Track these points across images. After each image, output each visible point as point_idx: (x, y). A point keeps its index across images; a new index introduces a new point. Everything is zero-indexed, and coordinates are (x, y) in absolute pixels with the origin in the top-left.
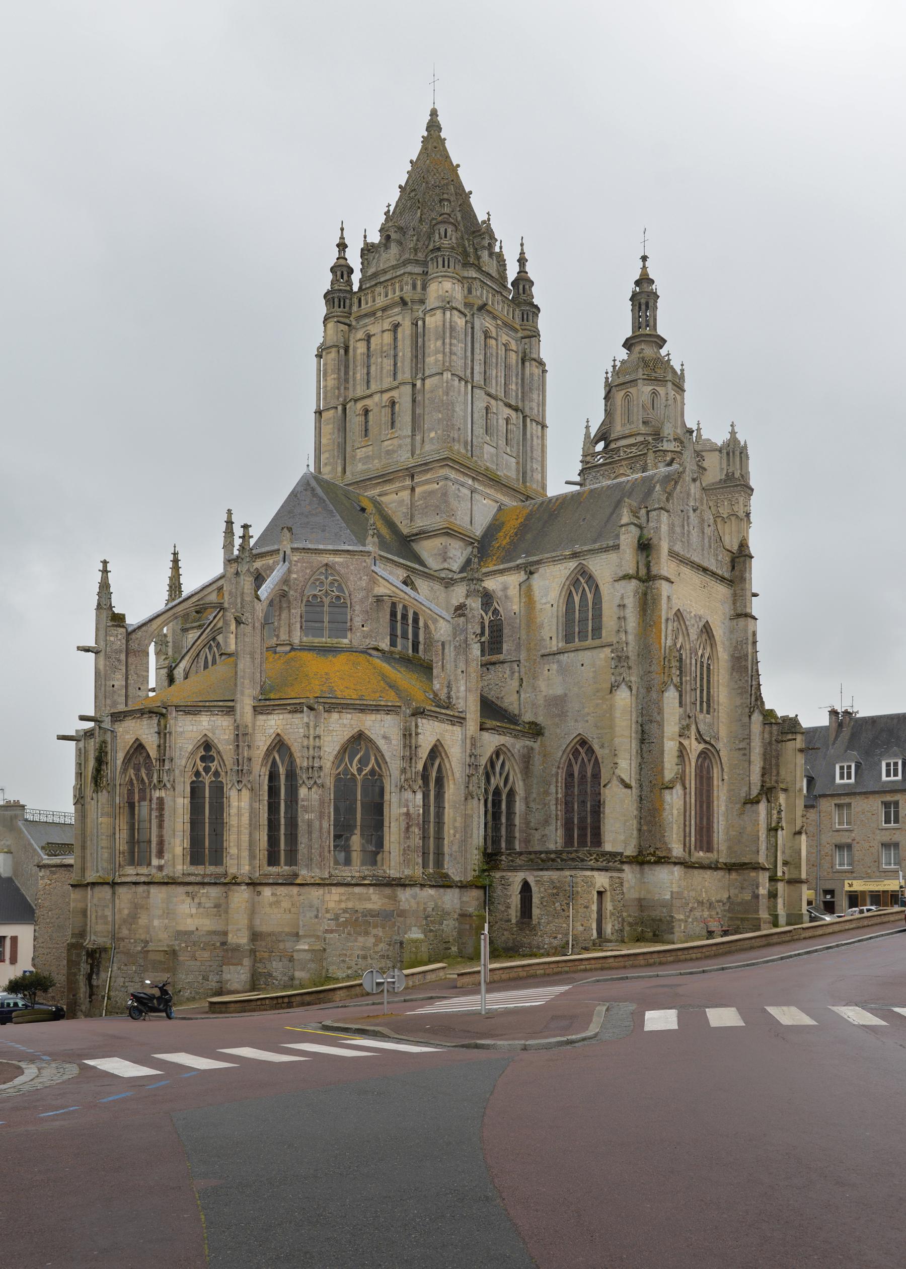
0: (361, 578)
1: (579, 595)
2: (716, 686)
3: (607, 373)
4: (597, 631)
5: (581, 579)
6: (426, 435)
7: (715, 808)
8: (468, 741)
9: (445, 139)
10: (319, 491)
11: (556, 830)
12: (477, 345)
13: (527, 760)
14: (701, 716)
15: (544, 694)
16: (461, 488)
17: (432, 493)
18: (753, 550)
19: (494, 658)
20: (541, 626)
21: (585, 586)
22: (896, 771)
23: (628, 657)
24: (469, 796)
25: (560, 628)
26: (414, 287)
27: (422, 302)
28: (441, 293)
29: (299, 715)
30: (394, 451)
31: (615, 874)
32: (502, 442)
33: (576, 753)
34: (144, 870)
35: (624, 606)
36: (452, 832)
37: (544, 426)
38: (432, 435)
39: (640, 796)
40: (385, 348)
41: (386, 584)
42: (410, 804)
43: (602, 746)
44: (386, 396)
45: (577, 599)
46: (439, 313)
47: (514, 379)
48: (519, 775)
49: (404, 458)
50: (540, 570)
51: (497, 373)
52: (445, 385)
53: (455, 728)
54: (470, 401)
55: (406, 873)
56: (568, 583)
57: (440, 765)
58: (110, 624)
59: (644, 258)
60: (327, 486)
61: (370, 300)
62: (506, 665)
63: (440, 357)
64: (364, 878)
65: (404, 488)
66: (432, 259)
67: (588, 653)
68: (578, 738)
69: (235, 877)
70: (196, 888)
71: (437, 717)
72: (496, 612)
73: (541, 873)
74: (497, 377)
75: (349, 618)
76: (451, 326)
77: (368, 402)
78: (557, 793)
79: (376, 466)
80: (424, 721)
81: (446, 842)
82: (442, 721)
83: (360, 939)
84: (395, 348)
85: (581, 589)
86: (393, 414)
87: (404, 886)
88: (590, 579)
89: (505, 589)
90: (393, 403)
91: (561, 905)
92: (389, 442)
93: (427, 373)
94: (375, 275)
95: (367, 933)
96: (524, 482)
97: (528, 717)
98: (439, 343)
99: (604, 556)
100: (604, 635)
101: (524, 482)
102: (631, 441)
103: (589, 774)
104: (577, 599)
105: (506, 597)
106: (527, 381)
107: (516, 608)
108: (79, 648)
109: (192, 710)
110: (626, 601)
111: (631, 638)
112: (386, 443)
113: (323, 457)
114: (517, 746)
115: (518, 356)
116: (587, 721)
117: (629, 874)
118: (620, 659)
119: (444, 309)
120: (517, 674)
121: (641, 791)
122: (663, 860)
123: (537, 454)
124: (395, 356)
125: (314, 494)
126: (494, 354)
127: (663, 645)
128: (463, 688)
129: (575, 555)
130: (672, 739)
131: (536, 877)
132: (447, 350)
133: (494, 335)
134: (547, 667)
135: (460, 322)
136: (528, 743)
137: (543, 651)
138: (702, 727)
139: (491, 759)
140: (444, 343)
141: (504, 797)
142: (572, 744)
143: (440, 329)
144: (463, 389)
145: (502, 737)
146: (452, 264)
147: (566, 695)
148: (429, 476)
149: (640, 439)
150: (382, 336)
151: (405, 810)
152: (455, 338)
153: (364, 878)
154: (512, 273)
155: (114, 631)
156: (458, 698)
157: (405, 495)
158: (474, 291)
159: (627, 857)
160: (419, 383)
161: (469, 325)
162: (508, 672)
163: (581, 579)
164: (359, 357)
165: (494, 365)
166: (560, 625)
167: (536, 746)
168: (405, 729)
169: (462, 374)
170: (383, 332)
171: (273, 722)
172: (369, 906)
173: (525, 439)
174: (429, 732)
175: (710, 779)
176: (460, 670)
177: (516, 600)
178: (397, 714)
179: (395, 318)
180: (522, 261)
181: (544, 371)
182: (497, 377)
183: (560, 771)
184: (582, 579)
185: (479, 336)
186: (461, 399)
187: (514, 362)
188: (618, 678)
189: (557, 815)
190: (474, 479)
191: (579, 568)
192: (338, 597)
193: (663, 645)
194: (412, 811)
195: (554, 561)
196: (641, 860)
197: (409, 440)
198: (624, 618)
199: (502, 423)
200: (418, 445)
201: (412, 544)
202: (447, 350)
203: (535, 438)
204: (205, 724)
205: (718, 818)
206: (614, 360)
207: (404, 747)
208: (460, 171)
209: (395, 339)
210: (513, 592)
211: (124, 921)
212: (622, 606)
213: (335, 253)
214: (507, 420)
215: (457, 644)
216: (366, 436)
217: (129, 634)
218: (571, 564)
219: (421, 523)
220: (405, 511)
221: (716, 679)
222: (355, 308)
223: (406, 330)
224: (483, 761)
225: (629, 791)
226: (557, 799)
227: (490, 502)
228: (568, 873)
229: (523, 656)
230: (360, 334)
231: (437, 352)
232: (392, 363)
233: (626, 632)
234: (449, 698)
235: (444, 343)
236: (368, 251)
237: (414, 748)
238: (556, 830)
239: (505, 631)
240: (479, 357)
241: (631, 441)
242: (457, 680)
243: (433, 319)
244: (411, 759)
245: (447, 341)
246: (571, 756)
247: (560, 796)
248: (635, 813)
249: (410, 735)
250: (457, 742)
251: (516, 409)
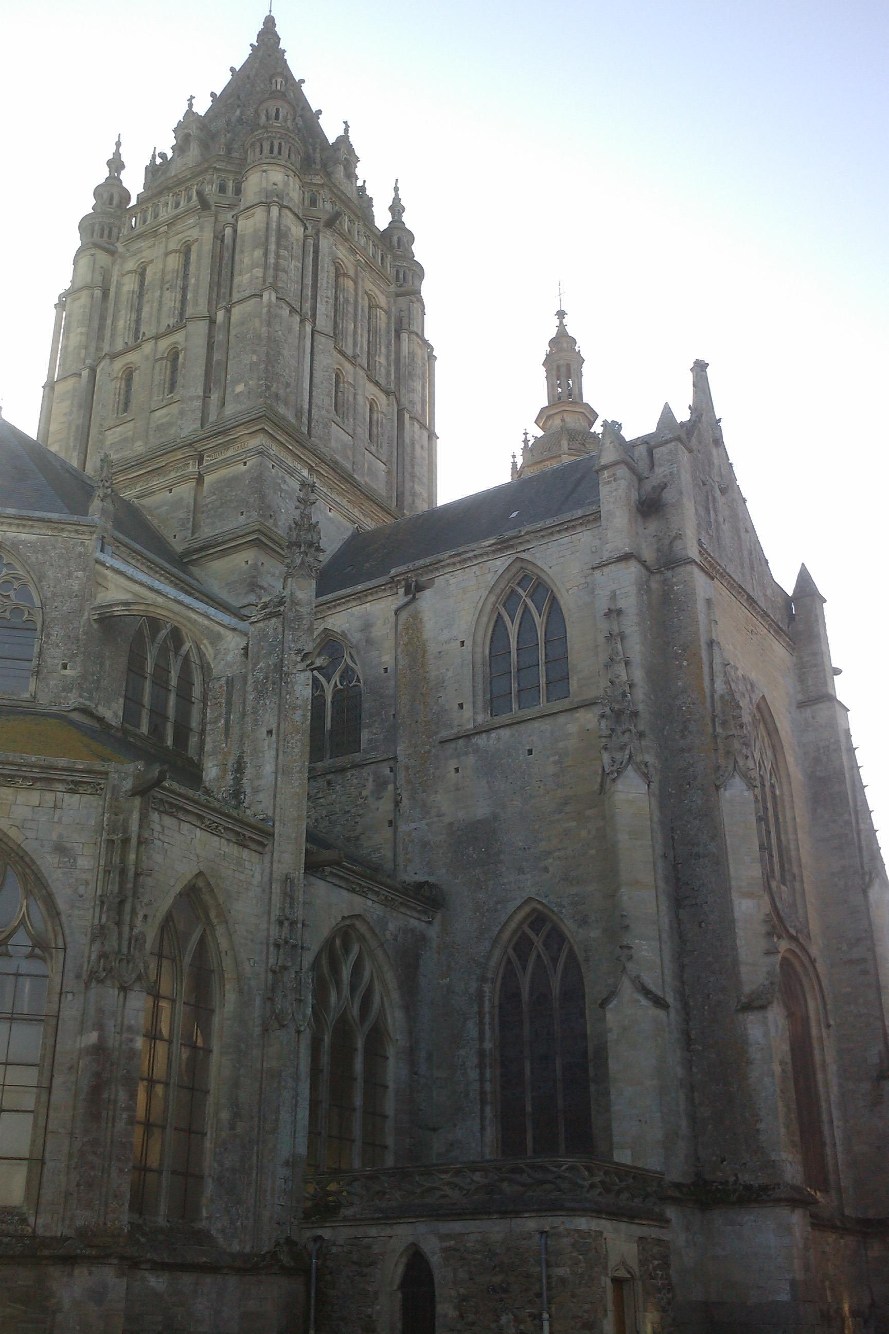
0: (70, 575)
1: (517, 620)
2: (790, 829)
3: (514, 457)
4: (559, 679)
5: (520, 590)
6: (228, 391)
7: (821, 1089)
8: (276, 888)
9: (284, 51)
11: (483, 1129)
13: (409, 960)
15: (447, 820)
16: (287, 477)
17: (233, 481)
18: (822, 590)
21: (529, 601)
23: (635, 714)
24: (274, 1021)
25: (480, 686)
26: (222, 189)
28: (264, 185)
31: (654, 1233)
33: (522, 946)
35: (619, 612)
36: (225, 1115)
38: (240, 388)
39: (686, 1034)
40: (167, 278)
41: (122, 580)
42: (110, 1024)
43: (584, 922)
44: (164, 344)
45: (513, 630)
46: (260, 213)
47: (383, 350)
48: (395, 995)
50: (439, 582)
52: (265, 310)
53: (245, 854)
54: (308, 350)
55: (79, 1223)
56: (493, 598)
57: (202, 942)
59: (561, 314)
62: (365, 771)
65: (184, 479)
66: (253, 144)
67: (545, 726)
68: (527, 909)
71: (201, 818)
72: (347, 674)
73: (457, 1227)
74: (355, 332)
75: (36, 650)
76: (279, 226)
78: (481, 1039)
80: (168, 821)
81: (208, 1144)
82: (213, 830)
84: (186, 276)
85: (520, 611)
86: (174, 370)
87: (69, 1261)
89: (367, 627)
91: (518, 1321)
92: (164, 411)
93: (236, 297)
97: (413, 874)
98: (258, 253)
99: (565, 539)
100: (574, 683)
104: (513, 630)
105: (369, 641)
107: (387, 659)
110: (622, 604)
111: (638, 675)
112: (158, 413)
114: (391, 926)
115: (389, 318)
116: (546, 869)
117: (678, 1230)
118: (620, 716)
119: (268, 206)
121: (687, 1021)
122: (755, 1196)
124: (184, 289)
126: (352, 300)
127: (707, 691)
128: (269, 768)
130: (750, 895)
131: (443, 1238)
132: (272, 260)
133: (351, 273)
134: (453, 764)
135: (297, 231)
136: (414, 923)
137: (444, 734)
139: (329, 945)
140: (266, 254)
141: (360, 1044)
142: (513, 925)
143: (262, 233)
144: (296, 327)
145: (357, 899)
146: (285, 151)
147: (495, 817)
150: (165, 261)
151: (93, 1037)
152: (286, 249)
154: (382, 220)
157: (185, 490)
158: (320, 203)
159: (677, 1186)
160: (220, 316)
161: (310, 241)
162: (370, 785)
163: (520, 590)
164: (124, 298)
165: (351, 316)
166: (479, 680)
167: (433, 932)
168: (113, 829)
169: (297, 306)
170: (167, 254)
174: (181, 850)
176: (264, 730)
177: (389, 644)
178: (97, 790)
179: (189, 232)
180: (396, 209)
182: (355, 332)
183: (487, 988)
187: (383, 326)
188: (618, 756)
189: (482, 1093)
191: (514, 570)
192: (17, 610)
193: (707, 691)
194: (113, 1041)
196: (709, 1194)
197: (198, 403)
198: (622, 636)
201: (194, 570)
202: (272, 260)
203: (417, 447)
205: (830, 1113)
206: (526, 434)
207: (107, 872)
208: (305, 88)
213: (105, 173)
215: (261, 676)
216: (125, 410)
218: (498, 562)
220: (182, 516)
221: (789, 815)
224: (314, 941)
225: (661, 1013)
226: (481, 1054)
227: (340, 518)
228: (531, 1224)
230: (131, 265)
231: (255, 266)
232: (179, 297)
233: (627, 663)
235: (266, 254)
237: (131, 874)
238: (483, 1129)
239: (366, 706)
243: (251, 222)
244: (122, 903)
245: (273, 247)
246: (510, 951)
247: (488, 1045)
248: (680, 1072)
249: (126, 841)
250: (251, 890)
251: (387, 393)
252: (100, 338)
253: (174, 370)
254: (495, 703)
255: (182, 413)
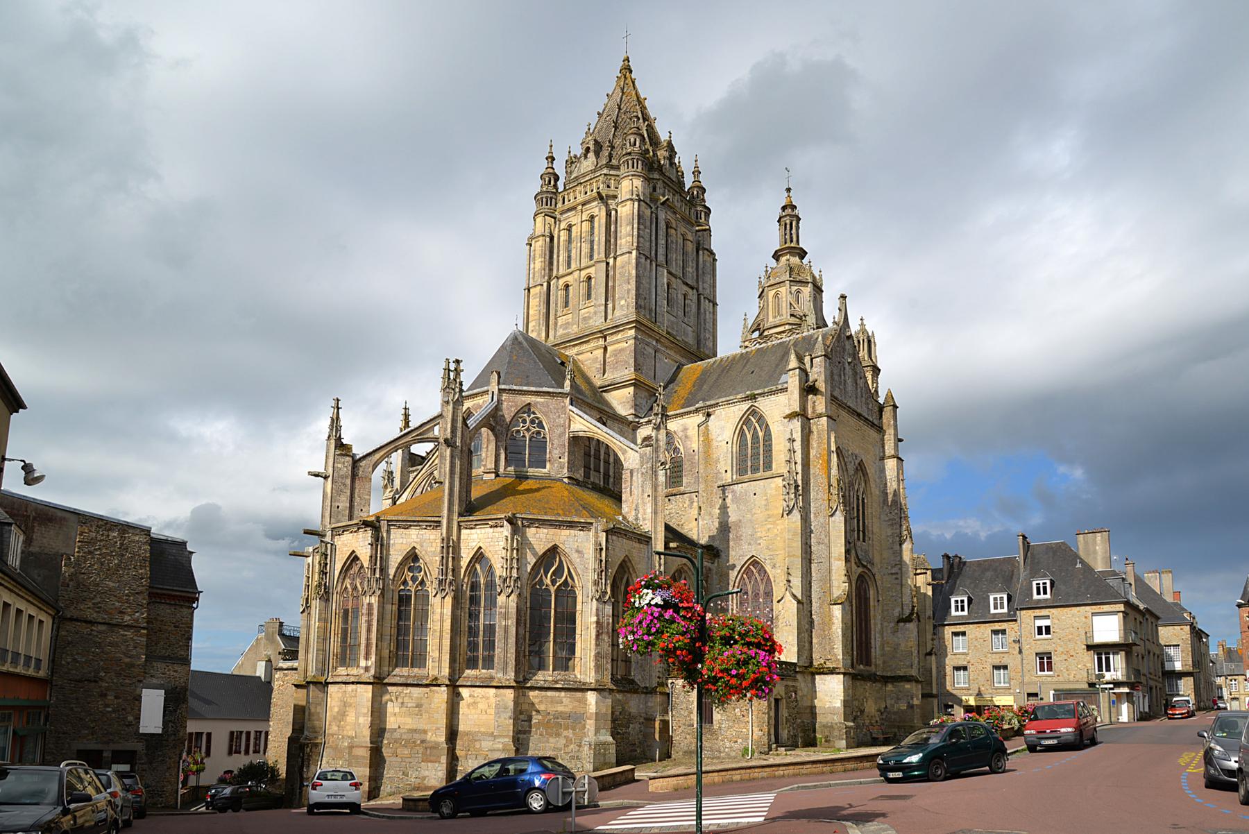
4: (768, 466)
10: (525, 344)
12: (660, 232)
14: (858, 544)
17: (622, 350)
19: (675, 490)
20: (718, 461)
22: (1002, 604)
27: (615, 197)
29: (499, 529)
30: (590, 318)
31: (790, 683)
32: (681, 313)
34: (354, 671)
37: (715, 304)
38: (623, 302)
43: (774, 567)
44: (584, 273)
45: (749, 437)
49: (598, 322)
51: (676, 257)
58: (338, 452)
60: (532, 342)
61: (571, 197)
63: (629, 239)
64: (556, 682)
65: (597, 348)
69: (436, 679)
70: (400, 688)
72: (676, 450)
77: (569, 279)
79: (574, 330)
83: (551, 740)
88: (761, 419)
90: (589, 278)
94: (576, 178)
95: (558, 735)
96: (698, 348)
98: (629, 228)
100: (774, 466)
101: (698, 348)
102: (781, 329)
103: (762, 592)
106: (701, 266)
107: (695, 446)
108: (310, 474)
109: (406, 525)
113: (530, 325)
120: (695, 504)
123: (709, 326)
125: (522, 348)
129: (746, 399)
138: (859, 553)
148: (620, 336)
149: (787, 327)
153: (556, 682)
154: (688, 182)
155: (342, 459)
156: (644, 519)
160: (611, 261)
167: (714, 567)
171: (475, 536)
172: (560, 709)
173: (698, 313)
175: (867, 600)
180: (697, 173)
181: (715, 260)
184: (753, 418)
185: (662, 225)
186: (647, 274)
190: (657, 341)
195: (729, 403)
199: (681, 297)
200: (610, 311)
204: (414, 537)
209: (592, 228)
210: (693, 432)
211: (335, 718)
212: (792, 440)
213: (545, 164)
214: (685, 296)
217: (356, 462)
219: (610, 376)
222: (559, 205)
223: (600, 222)
229: (701, 487)
230: (563, 225)
234: (637, 519)
236: (571, 162)
240: (662, 242)
241: (781, 329)
242: (644, 503)
251: (692, 288)
252: (551, 270)
253: (589, 288)
254: (741, 470)
255: (595, 313)
